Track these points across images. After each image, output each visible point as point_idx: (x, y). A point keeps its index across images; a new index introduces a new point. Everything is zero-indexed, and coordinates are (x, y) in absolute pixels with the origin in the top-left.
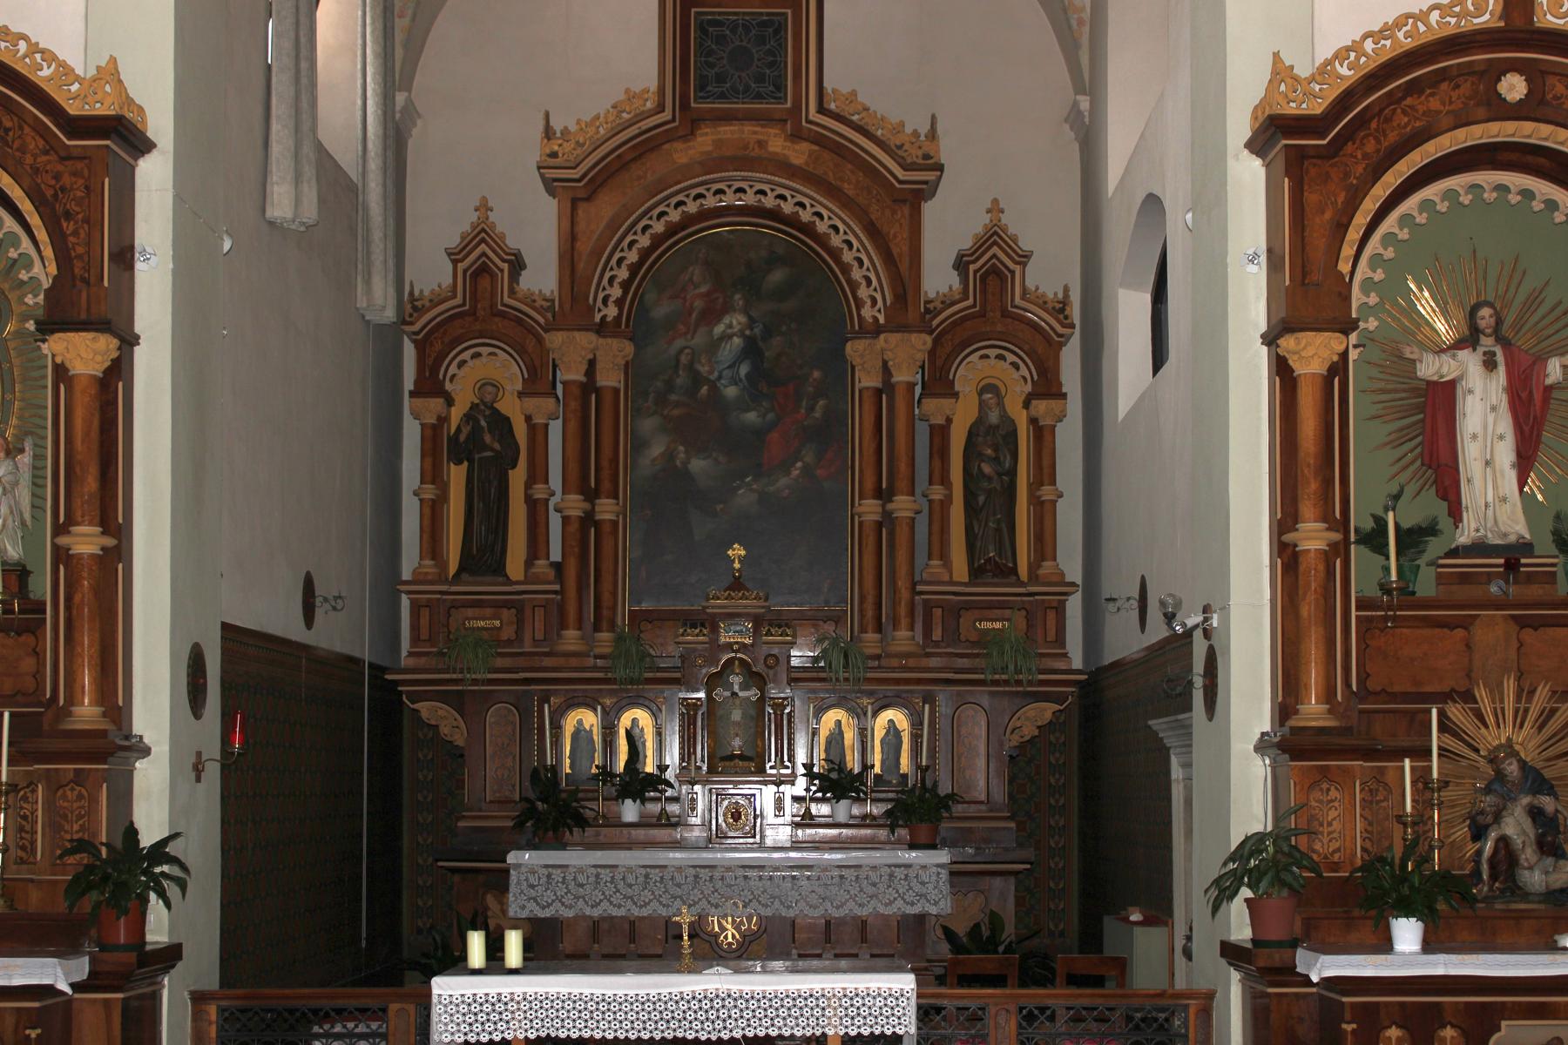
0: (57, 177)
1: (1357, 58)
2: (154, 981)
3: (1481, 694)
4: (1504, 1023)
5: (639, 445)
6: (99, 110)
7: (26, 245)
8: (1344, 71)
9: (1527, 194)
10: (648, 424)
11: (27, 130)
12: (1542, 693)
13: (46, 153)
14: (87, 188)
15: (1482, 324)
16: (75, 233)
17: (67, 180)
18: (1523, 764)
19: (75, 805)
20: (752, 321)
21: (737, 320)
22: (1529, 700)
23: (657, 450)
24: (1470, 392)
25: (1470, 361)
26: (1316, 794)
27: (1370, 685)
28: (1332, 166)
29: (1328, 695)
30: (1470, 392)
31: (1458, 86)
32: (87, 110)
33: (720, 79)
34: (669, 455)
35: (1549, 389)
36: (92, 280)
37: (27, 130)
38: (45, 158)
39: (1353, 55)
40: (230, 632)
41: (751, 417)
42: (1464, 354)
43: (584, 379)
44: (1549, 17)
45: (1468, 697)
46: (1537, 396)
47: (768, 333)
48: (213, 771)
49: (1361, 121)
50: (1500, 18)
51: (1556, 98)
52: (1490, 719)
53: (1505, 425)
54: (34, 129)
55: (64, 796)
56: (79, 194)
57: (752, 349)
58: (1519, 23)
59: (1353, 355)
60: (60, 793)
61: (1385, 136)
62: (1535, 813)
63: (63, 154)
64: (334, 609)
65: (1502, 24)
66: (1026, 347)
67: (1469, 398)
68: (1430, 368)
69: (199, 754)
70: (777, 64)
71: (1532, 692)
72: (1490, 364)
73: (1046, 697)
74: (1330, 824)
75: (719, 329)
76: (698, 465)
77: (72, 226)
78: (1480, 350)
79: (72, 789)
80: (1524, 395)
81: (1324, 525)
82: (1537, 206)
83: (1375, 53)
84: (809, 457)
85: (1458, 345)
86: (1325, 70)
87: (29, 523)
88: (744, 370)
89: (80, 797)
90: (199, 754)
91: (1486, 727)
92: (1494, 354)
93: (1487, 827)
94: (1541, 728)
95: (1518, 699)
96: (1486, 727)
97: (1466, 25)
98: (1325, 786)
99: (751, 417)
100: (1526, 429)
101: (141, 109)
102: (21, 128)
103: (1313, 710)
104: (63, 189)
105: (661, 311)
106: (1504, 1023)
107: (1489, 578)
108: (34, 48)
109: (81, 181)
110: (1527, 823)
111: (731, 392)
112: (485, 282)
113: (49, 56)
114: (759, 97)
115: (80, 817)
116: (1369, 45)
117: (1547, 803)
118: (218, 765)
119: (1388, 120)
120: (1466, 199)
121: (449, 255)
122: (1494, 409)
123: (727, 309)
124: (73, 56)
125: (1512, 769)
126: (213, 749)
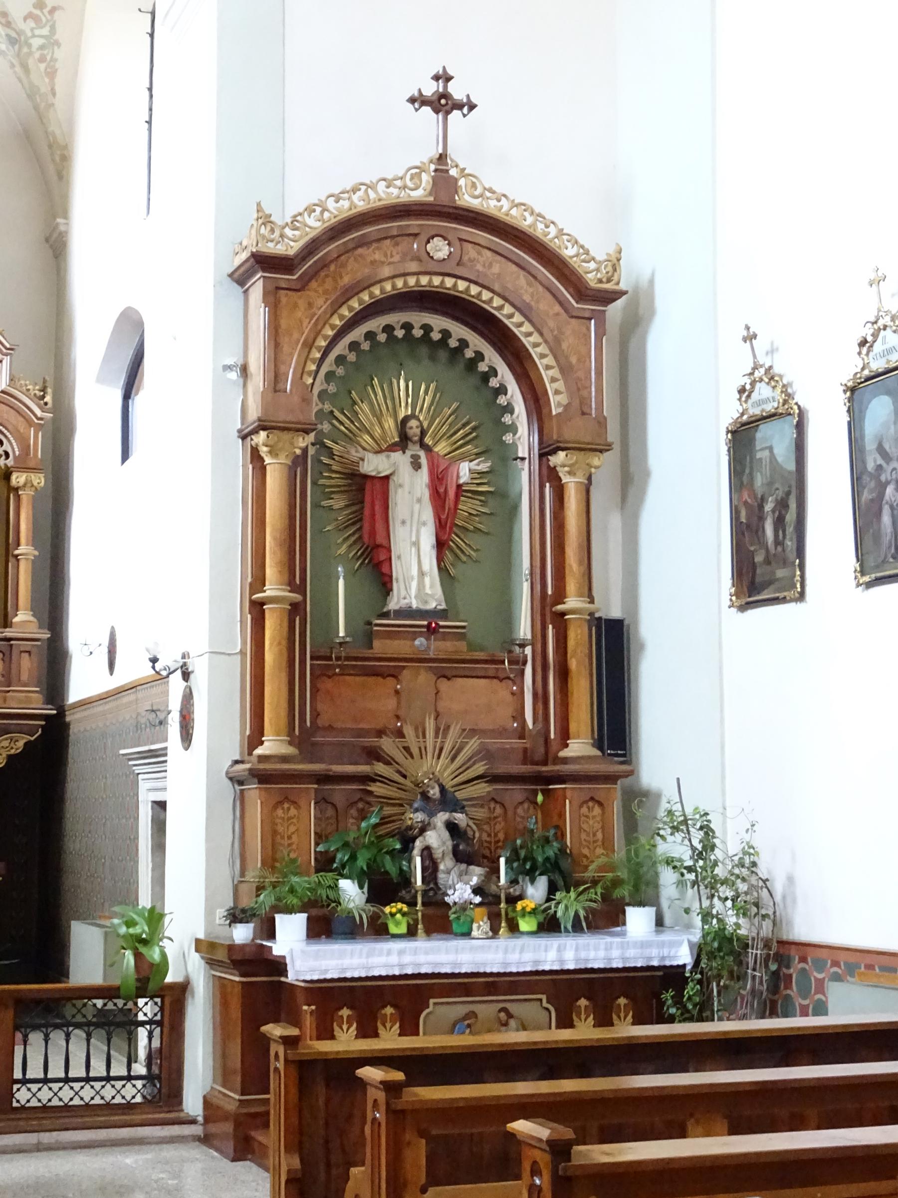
1: (322, 213)
3: (409, 731)
4: (432, 1001)
15: (410, 433)
22: (445, 736)
24: (401, 486)
25: (401, 460)
26: (280, 812)
27: (320, 722)
28: (300, 298)
30: (401, 486)
31: (397, 244)
35: (459, 486)
39: (318, 209)
42: (397, 456)
43: (586, 482)
44: (466, 197)
49: (323, 265)
50: (430, 194)
51: (470, 260)
52: (415, 751)
58: (444, 200)
59: (311, 451)
61: (341, 277)
62: (452, 827)
65: (431, 199)
66: (10, 427)
67: (400, 491)
68: (374, 465)
71: (447, 728)
72: (416, 465)
74: (289, 837)
78: (409, 453)
80: (442, 490)
81: (289, 588)
82: (352, 357)
85: (392, 448)
86: (294, 223)
91: (412, 757)
92: (419, 457)
93: (413, 839)
94: (453, 759)
95: (436, 736)
96: (412, 757)
98: (286, 805)
100: (443, 517)
106: (432, 1001)
107: (415, 636)
110: (446, 835)
116: (382, 186)
117: (460, 818)
119: (343, 266)
122: (419, 501)
125: (434, 792)
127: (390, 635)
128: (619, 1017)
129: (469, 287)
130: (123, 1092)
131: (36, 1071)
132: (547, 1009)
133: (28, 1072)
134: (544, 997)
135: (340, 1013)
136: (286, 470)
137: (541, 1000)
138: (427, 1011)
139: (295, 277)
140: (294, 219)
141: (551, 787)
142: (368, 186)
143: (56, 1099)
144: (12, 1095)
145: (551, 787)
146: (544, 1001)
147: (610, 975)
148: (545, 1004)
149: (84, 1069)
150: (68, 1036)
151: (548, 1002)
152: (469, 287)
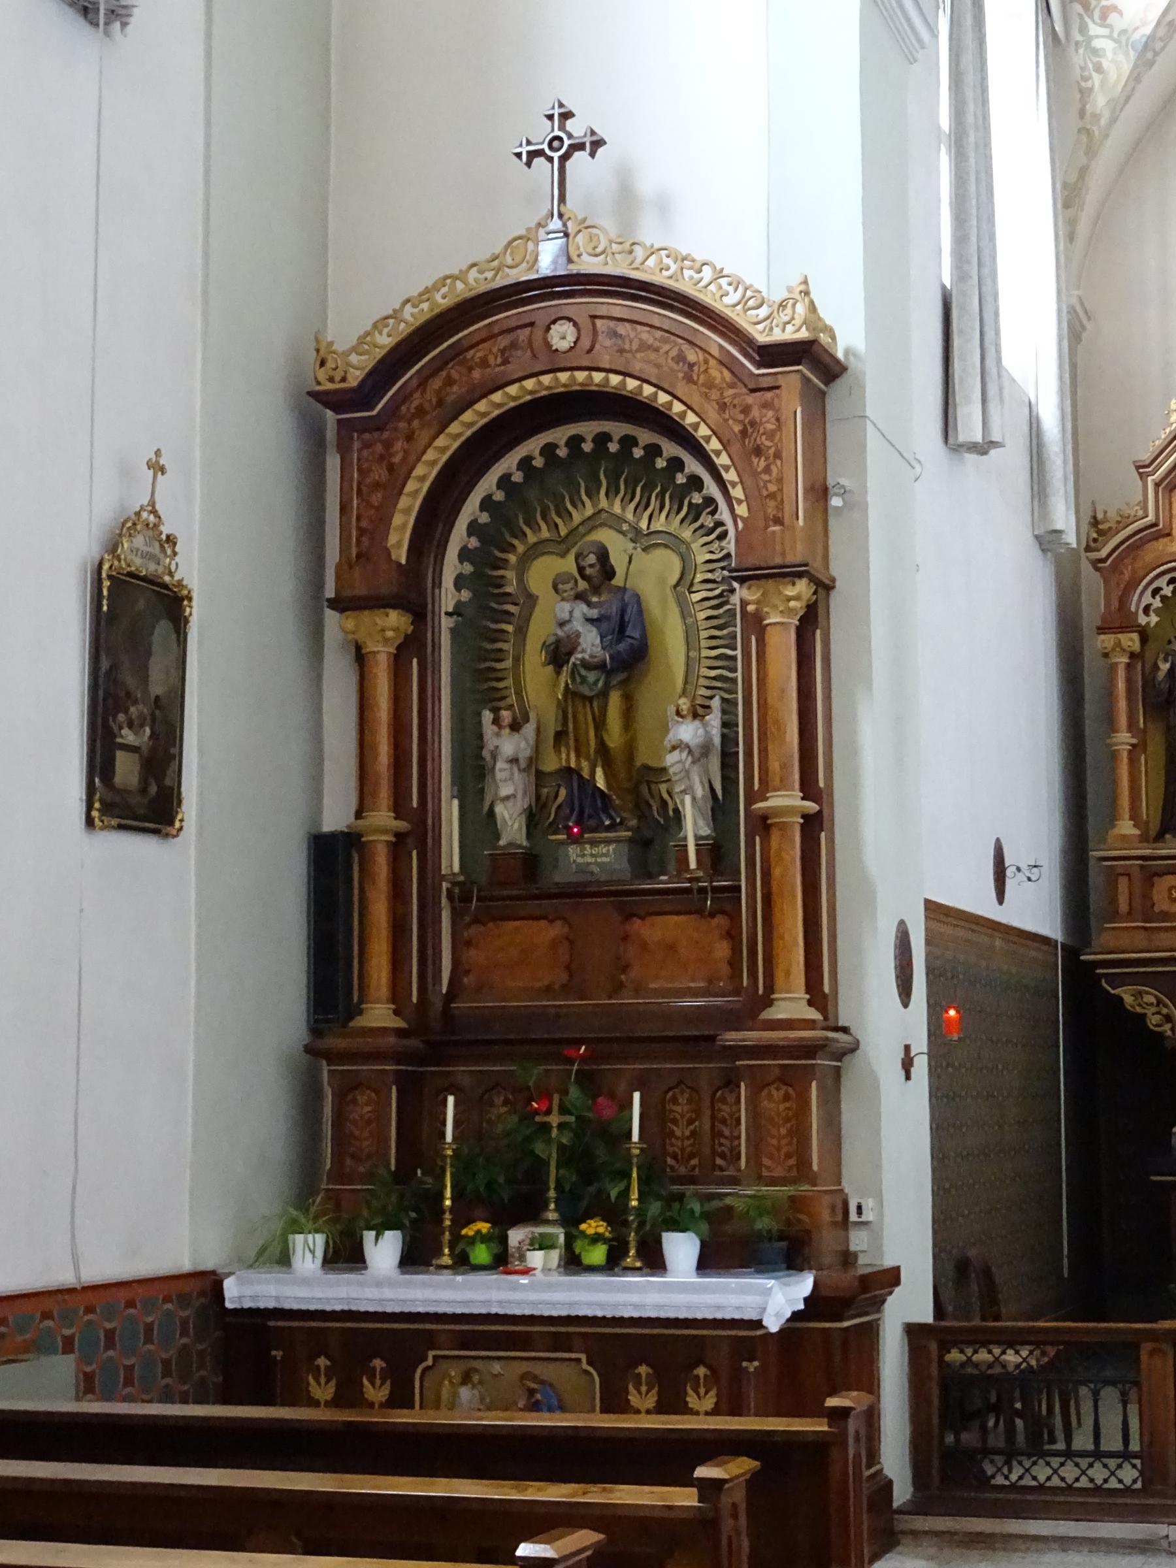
0: (746, 410)
2: (878, 1304)
4: (431, 1354)
6: (789, 334)
9: (460, 582)
11: (712, 362)
13: (732, 386)
14: (778, 420)
16: (767, 470)
17: (755, 413)
19: (782, 1107)
29: (397, 995)
32: (778, 336)
36: (787, 520)
37: (712, 362)
38: (731, 392)
40: (934, 910)
48: (921, 1066)
54: (721, 363)
55: (770, 1096)
56: (770, 427)
60: (765, 1093)
63: (752, 386)
64: (1029, 879)
69: (907, 1048)
77: (762, 464)
79: (778, 1089)
81: (392, 814)
87: (720, 797)
89: (787, 1098)
90: (907, 1048)
101: (830, 331)
102: (706, 362)
104: (753, 423)
106: (431, 1354)
108: (719, 274)
109: (770, 413)
115: (369, 1122)
118: (925, 1057)
121: (1138, 468)
124: (755, 278)
126: (920, 1045)
127: (451, 866)
128: (373, 1384)
129: (656, 393)
130: (1077, 1472)
131: (1082, 1441)
132: (587, 1372)
133: (1102, 1441)
134: (583, 1357)
135: (695, 1372)
136: (392, 659)
137: (579, 1360)
138: (424, 1365)
139: (374, 413)
140: (361, 340)
141: (603, 1067)
142: (457, 278)
143: (1084, 1479)
144: (1142, 1473)
145: (603, 1067)
146: (584, 1360)
147: (428, 1326)
148: (585, 1366)
149: (1119, 1437)
150: (1096, 1394)
151: (589, 1363)
152: (656, 393)
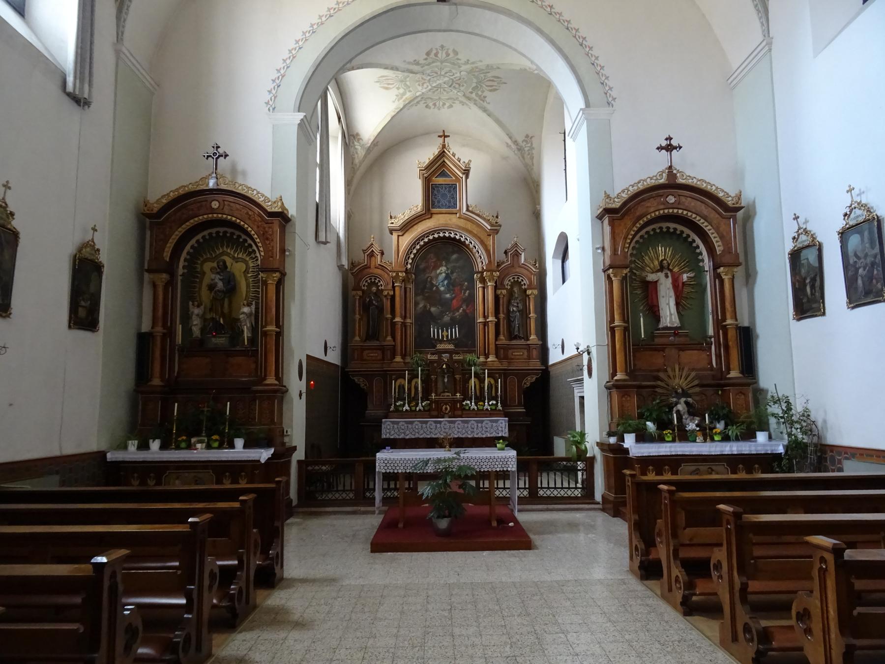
3: (669, 370)
5: (416, 304)
6: (276, 210)
7: (254, 247)
8: (624, 195)
10: (419, 298)
12: (686, 369)
18: (683, 390)
20: (448, 269)
21: (443, 269)
23: (421, 305)
25: (661, 275)
32: (273, 210)
33: (450, 202)
34: (425, 307)
35: (683, 283)
41: (448, 296)
42: (659, 274)
45: (666, 371)
46: (681, 285)
47: (452, 273)
48: (304, 396)
49: (629, 210)
53: (672, 293)
57: (447, 277)
58: (672, 182)
62: (686, 403)
68: (651, 277)
70: (454, 198)
71: (683, 369)
72: (667, 276)
73: (534, 374)
75: (438, 271)
76: (433, 309)
83: (633, 190)
84: (465, 307)
86: (618, 196)
88: (446, 282)
97: (657, 183)
99: (448, 296)
103: (619, 376)
105: (422, 266)
111: (442, 289)
112: (373, 259)
113: (263, 195)
114: (449, 207)
120: (658, 231)
123: (441, 265)
124: (268, 195)
126: (304, 390)
